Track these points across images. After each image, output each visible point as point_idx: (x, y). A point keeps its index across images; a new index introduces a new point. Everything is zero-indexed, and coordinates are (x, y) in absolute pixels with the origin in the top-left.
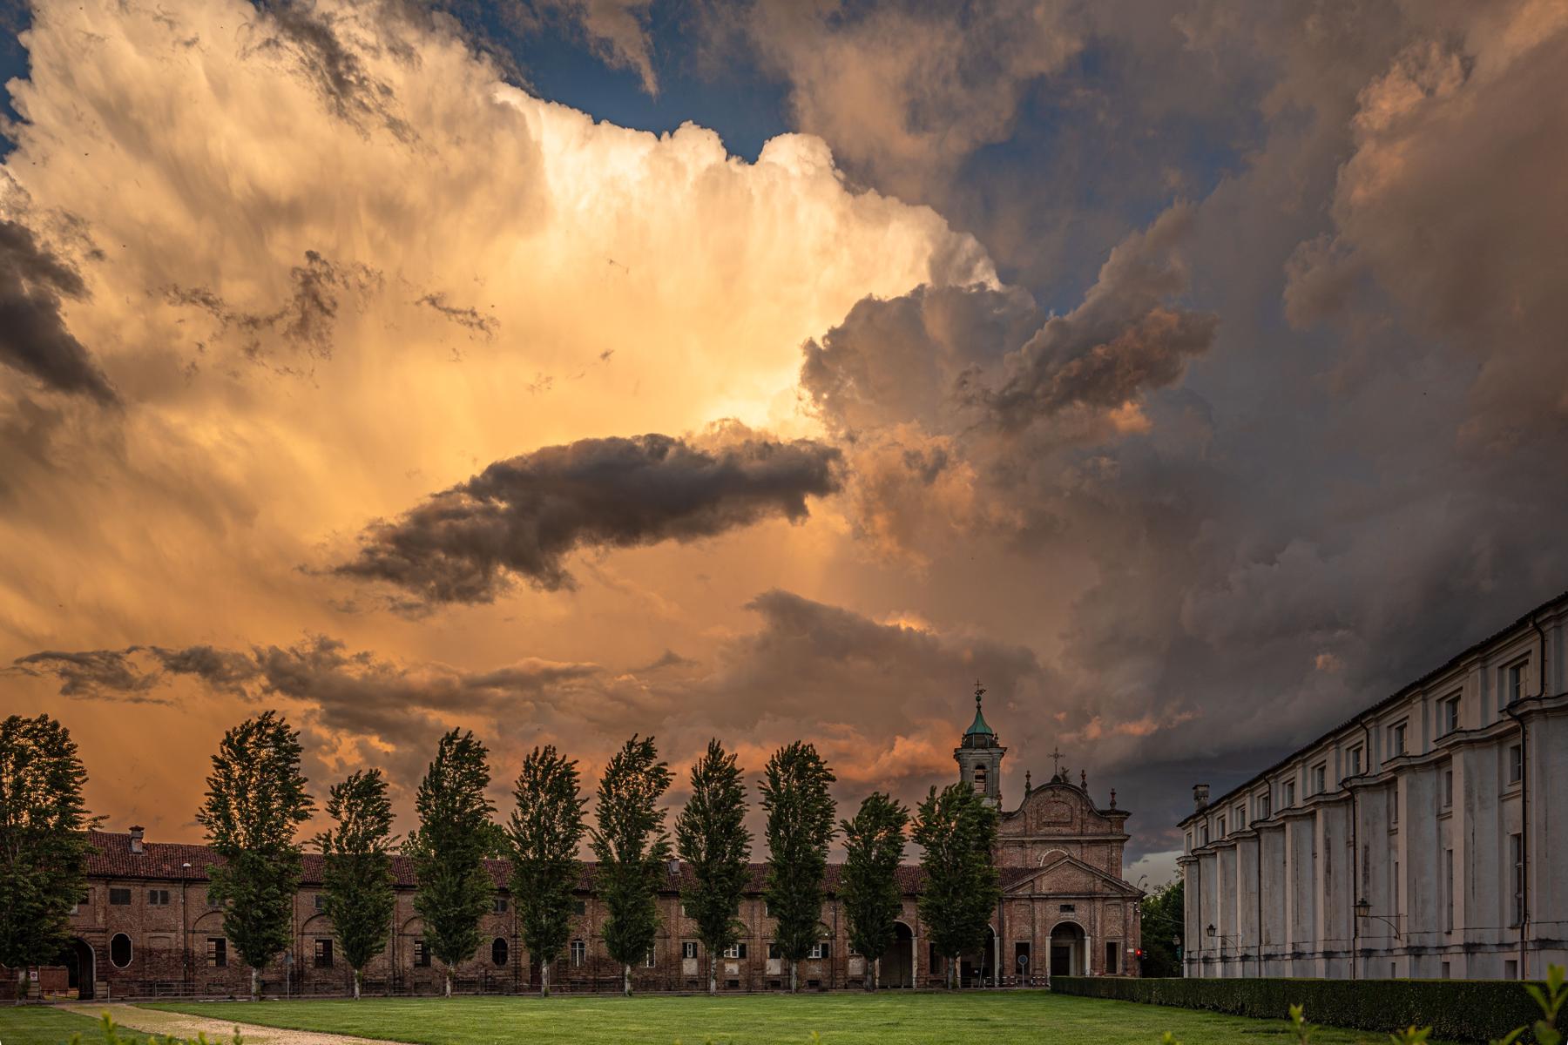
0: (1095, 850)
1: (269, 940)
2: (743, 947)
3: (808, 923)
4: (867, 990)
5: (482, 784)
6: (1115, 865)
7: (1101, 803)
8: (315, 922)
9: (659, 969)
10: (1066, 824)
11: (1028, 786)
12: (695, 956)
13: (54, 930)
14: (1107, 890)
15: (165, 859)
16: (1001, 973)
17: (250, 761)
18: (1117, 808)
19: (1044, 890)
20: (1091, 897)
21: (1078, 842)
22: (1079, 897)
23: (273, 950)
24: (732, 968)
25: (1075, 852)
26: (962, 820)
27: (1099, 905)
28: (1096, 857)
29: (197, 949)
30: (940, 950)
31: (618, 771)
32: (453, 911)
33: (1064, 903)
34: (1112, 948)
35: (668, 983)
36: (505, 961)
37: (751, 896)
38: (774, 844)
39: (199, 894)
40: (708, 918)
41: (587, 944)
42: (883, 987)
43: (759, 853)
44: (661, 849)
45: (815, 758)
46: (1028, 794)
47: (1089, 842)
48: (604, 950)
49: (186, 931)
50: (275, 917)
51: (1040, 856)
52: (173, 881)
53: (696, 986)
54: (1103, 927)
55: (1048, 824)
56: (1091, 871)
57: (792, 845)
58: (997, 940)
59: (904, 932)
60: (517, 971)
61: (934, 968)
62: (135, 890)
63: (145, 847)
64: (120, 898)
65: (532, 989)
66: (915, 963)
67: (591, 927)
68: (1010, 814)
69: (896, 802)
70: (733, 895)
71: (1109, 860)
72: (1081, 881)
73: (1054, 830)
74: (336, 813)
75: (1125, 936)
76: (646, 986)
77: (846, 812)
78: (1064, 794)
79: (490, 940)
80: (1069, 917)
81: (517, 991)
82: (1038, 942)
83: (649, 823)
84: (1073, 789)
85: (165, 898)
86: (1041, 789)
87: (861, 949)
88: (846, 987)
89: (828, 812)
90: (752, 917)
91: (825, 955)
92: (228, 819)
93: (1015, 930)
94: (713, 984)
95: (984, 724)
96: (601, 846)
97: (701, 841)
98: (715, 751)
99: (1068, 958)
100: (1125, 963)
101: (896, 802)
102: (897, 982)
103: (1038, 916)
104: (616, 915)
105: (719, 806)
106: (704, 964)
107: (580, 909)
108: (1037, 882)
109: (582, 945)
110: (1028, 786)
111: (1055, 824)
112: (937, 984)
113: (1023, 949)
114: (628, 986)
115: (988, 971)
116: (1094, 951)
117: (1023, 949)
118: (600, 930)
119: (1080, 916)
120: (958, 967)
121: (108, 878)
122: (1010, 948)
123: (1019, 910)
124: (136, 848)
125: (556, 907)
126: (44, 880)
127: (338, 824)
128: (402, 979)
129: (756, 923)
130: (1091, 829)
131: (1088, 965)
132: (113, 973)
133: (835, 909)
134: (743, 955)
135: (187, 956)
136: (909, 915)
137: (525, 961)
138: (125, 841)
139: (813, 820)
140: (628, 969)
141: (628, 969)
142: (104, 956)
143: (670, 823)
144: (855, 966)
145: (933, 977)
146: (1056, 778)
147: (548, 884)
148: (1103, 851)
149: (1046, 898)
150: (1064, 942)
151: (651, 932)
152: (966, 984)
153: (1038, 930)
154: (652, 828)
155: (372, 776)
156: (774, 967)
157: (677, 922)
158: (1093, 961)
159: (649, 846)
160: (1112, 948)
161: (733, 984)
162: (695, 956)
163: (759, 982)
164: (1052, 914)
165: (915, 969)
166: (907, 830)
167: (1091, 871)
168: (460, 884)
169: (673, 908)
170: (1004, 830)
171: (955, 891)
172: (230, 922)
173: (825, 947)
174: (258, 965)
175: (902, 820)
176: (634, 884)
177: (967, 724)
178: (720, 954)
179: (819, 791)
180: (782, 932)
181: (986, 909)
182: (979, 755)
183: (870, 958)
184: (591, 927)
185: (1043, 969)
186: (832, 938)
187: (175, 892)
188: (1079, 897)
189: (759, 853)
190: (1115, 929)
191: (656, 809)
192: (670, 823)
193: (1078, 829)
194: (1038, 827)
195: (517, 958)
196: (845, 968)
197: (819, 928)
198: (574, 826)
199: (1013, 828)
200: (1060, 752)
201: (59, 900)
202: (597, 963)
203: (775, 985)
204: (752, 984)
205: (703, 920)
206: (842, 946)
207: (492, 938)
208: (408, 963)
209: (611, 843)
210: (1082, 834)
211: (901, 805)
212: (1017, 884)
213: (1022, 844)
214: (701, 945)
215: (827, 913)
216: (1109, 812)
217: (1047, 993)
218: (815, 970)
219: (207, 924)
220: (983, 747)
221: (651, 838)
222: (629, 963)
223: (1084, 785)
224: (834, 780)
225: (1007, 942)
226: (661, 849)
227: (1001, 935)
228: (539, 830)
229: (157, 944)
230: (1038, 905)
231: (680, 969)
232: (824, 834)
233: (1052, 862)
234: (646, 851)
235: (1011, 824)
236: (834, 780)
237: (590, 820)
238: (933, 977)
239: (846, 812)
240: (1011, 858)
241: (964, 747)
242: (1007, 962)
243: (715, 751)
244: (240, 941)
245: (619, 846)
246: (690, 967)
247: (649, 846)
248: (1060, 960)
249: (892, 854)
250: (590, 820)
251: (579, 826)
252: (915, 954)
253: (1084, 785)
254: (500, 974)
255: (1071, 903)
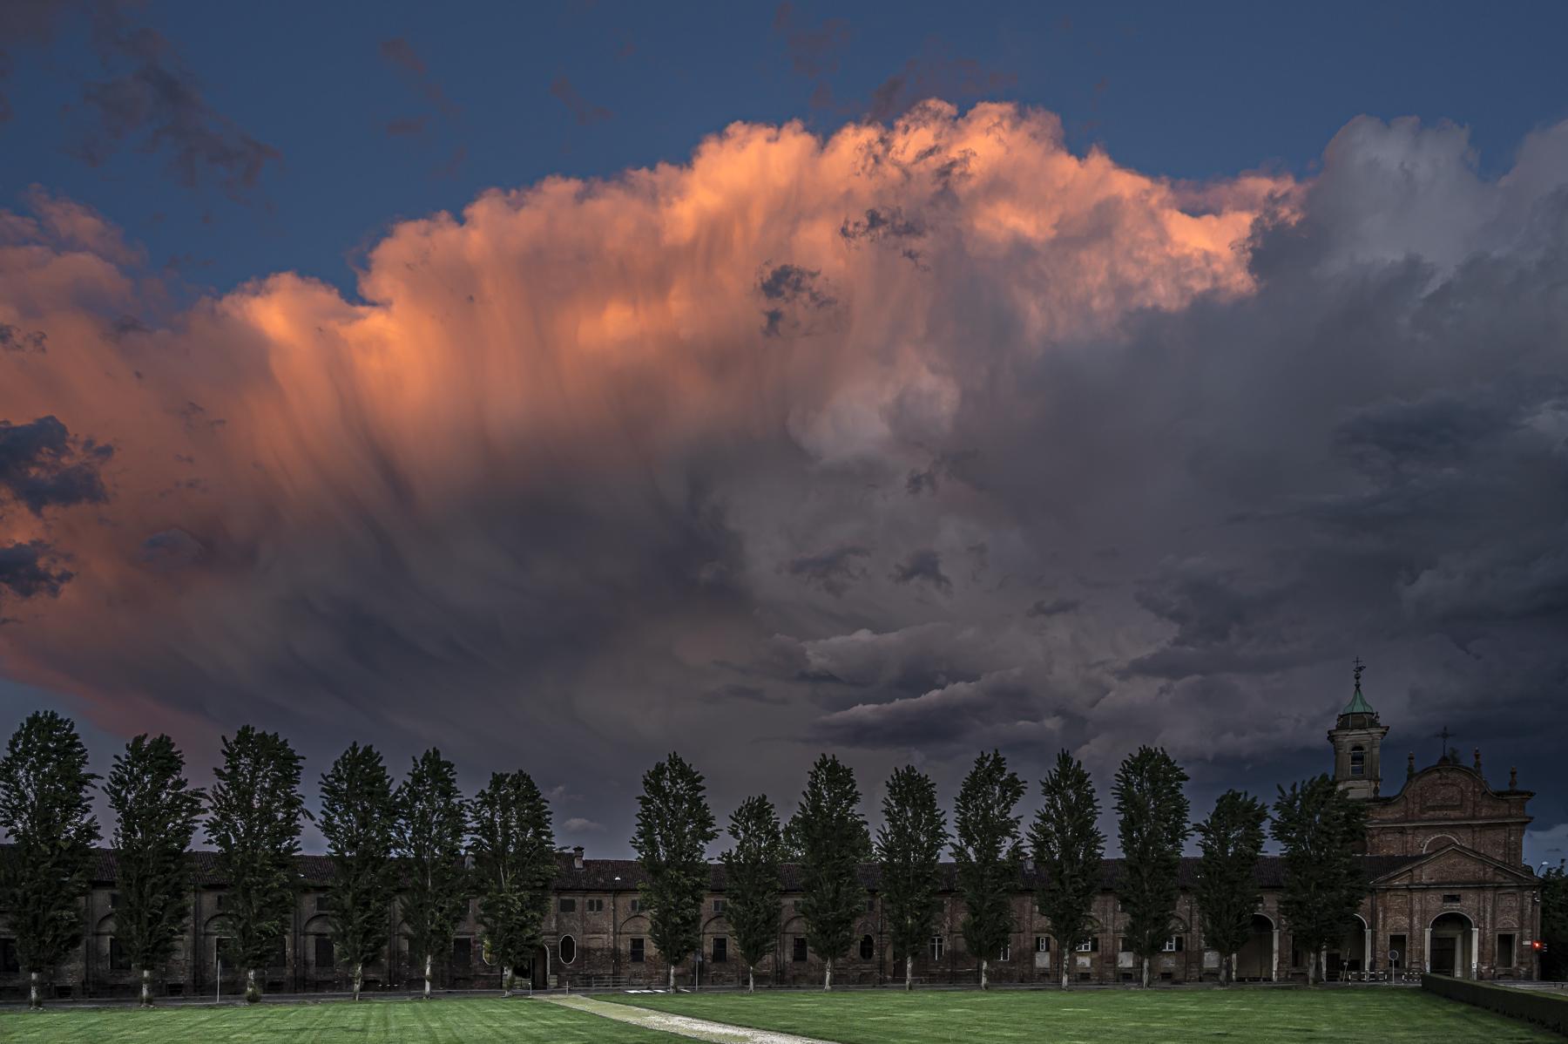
0: (1490, 834)
1: (685, 942)
2: (1095, 941)
3: (1161, 921)
4: (1222, 984)
5: (853, 800)
6: (1514, 850)
7: (1498, 784)
8: (713, 924)
9: (1012, 962)
10: (1453, 808)
11: (1410, 769)
12: (1048, 949)
13: (533, 938)
14: (1500, 879)
15: (599, 873)
16: (1372, 967)
17: (666, 796)
18: (1518, 788)
19: (1425, 879)
20: (1480, 886)
21: (1469, 826)
22: (1467, 885)
23: (687, 951)
24: (1084, 961)
25: (1463, 840)
26: (1326, 814)
27: (1489, 895)
28: (1491, 844)
29: (622, 947)
30: (1301, 945)
31: (975, 787)
32: (831, 915)
33: (1447, 893)
34: (1506, 940)
35: (1021, 976)
36: (871, 955)
37: (1106, 891)
38: (1128, 846)
39: (624, 901)
40: (1062, 917)
41: (946, 939)
42: (1240, 980)
43: (1112, 850)
44: (1016, 851)
45: (1166, 760)
46: (1409, 778)
47: (1482, 826)
48: (962, 944)
49: (615, 933)
50: (691, 923)
51: (1424, 843)
52: (606, 891)
53: (1047, 979)
54: (1493, 919)
55: (1433, 808)
56: (1483, 859)
57: (1145, 844)
58: (1368, 932)
59: (1263, 924)
60: (882, 966)
61: (1296, 962)
62: (579, 900)
63: (586, 863)
64: (567, 907)
65: (894, 981)
66: (1275, 956)
67: (952, 922)
68: (1388, 799)
69: (1254, 799)
70: (1086, 894)
71: (1506, 845)
72: (1470, 869)
73: (1439, 814)
74: (735, 834)
75: (1522, 926)
76: (1000, 980)
77: (1199, 813)
78: (1453, 775)
79: (859, 938)
80: (1455, 907)
81: (882, 983)
82: (1416, 933)
83: (1006, 828)
84: (1467, 771)
85: (600, 906)
86: (1427, 771)
87: (1214, 944)
88: (1201, 980)
89: (1181, 811)
90: (1105, 912)
91: (1179, 948)
92: (652, 844)
93: (1389, 921)
94: (1065, 979)
95: (1364, 703)
96: (960, 852)
97: (1055, 847)
98: (1065, 759)
99: (1453, 950)
100: (1520, 956)
101: (1254, 799)
102: (1257, 975)
103: (1417, 907)
104: (974, 915)
105: (1071, 809)
106: (1057, 958)
107: (941, 908)
108: (1416, 872)
109: (940, 941)
111: (1441, 808)
112: (1295, 979)
113: (1398, 941)
114: (984, 980)
115: (1357, 965)
116: (1482, 943)
117: (1398, 941)
118: (958, 926)
119: (1468, 905)
120: (1323, 960)
121: (560, 891)
122: (1384, 939)
123: (1394, 901)
124: (578, 864)
125: (920, 908)
126: (526, 897)
127: (738, 842)
128: (783, 972)
129: (1109, 917)
130: (1484, 812)
131: (1473, 960)
132: (562, 967)
133: (1190, 903)
134: (1095, 948)
135: (615, 953)
136: (1269, 906)
137: (889, 955)
138: (570, 858)
139: (1167, 820)
140: (985, 965)
141: (985, 965)
142: (554, 954)
143: (1024, 830)
144: (1211, 959)
145: (1295, 970)
146: (1444, 759)
147: (913, 880)
148: (1501, 836)
149: (1427, 888)
150: (1448, 932)
151: (1007, 931)
152: (1332, 976)
153: (1416, 920)
154: (1008, 834)
155: (763, 799)
156: (1126, 961)
157: (1031, 917)
158: (1480, 954)
159: (1005, 850)
160: (1506, 940)
161: (1085, 977)
162: (1048, 949)
163: (1110, 974)
164: (1435, 904)
165: (1275, 963)
166: (1266, 827)
167: (1483, 859)
168: (837, 892)
169: (1028, 905)
170: (1377, 818)
171: (1319, 886)
172: (655, 927)
173: (1179, 940)
174: (676, 963)
175: (1261, 816)
176: (992, 884)
178: (1072, 950)
179: (1173, 791)
180: (1132, 929)
181: (1353, 903)
183: (1225, 952)
184: (952, 922)
185: (1421, 961)
186: (1188, 930)
187: (607, 900)
188: (1467, 885)
189: (1112, 850)
190: (1509, 921)
191: (1011, 816)
192: (1024, 830)
193: (1469, 812)
194: (1422, 811)
195: (882, 953)
196: (1200, 961)
197: (1173, 923)
198: (936, 837)
199: (1391, 813)
201: (537, 915)
202: (954, 956)
203: (1127, 977)
204: (1108, 977)
205: (1056, 919)
206: (1196, 939)
207: (861, 937)
208: (788, 958)
209: (970, 850)
210: (1474, 818)
211: (1259, 803)
212: (1393, 874)
213: (1402, 831)
214: (1054, 942)
215: (1184, 906)
216: (1509, 793)
217: (1414, 991)
218: (1169, 963)
219: (630, 927)
220: (1361, 728)
221: (1007, 844)
222: (986, 957)
223: (1478, 765)
224: (1186, 779)
225: (1380, 936)
226: (1016, 851)
227: (1373, 926)
228: (901, 840)
229: (594, 944)
230: (1417, 896)
231: (1032, 961)
232: (1177, 834)
233: (1437, 848)
234: (1002, 856)
235: (1390, 809)
236: (1186, 779)
237: (951, 828)
238: (1295, 970)
239: (1199, 813)
240: (1391, 846)
241: (1339, 728)
242: (1380, 955)
243: (1065, 759)
244: (661, 943)
245: (976, 851)
246: (1043, 960)
247: (1005, 850)
248: (1443, 955)
249: (1251, 850)
250: (951, 828)
251: (940, 835)
252: (1276, 946)
253: (1478, 765)
254: (866, 967)
255: (1455, 893)
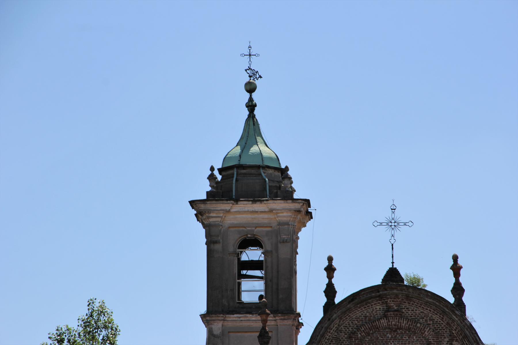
11: (330, 291)
46: (329, 307)
110: (330, 291)
177: (221, 145)
182: (243, 214)
200: (400, 215)
253: (458, 290)
